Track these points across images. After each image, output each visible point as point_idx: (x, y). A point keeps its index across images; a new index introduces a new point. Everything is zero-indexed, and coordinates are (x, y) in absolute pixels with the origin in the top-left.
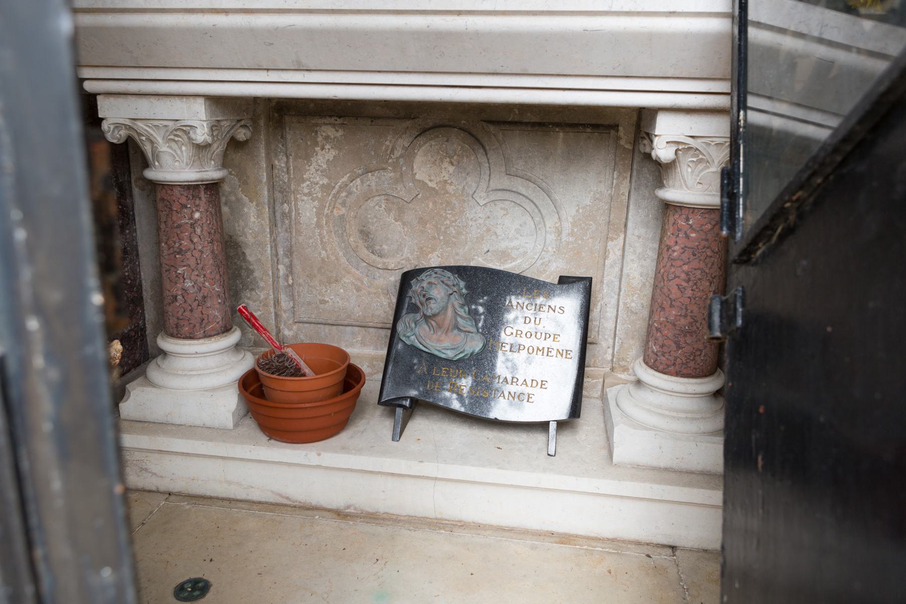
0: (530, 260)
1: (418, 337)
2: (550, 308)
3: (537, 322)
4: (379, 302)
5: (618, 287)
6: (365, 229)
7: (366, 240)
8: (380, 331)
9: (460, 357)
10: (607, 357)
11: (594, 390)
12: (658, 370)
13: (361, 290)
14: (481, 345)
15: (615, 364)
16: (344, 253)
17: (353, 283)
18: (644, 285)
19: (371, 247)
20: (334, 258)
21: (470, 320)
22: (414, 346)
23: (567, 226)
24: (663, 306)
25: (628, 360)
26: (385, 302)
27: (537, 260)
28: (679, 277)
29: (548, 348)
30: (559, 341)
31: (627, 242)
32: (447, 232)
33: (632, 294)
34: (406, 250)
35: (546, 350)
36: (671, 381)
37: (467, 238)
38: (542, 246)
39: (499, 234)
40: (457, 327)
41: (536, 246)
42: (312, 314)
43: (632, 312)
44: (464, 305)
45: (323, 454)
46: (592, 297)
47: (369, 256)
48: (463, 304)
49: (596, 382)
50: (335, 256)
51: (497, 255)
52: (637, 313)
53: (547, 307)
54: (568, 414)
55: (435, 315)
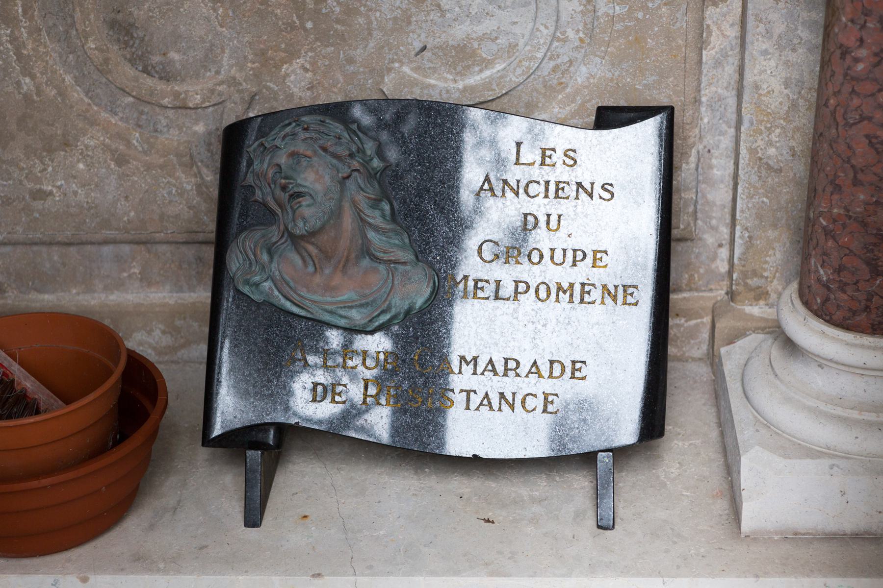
0: (524, 63)
1: (279, 284)
2: (580, 190)
3: (553, 224)
4: (175, 186)
5: (734, 109)
6: (120, 17)
7: (126, 43)
8: (184, 248)
9: (381, 322)
10: (717, 267)
11: (692, 342)
13: (128, 162)
14: (427, 292)
15: (737, 285)
16: (75, 77)
17: (106, 148)
18: (794, 106)
19: (141, 58)
20: (54, 92)
21: (397, 233)
22: (272, 305)
24: (837, 182)
25: (765, 274)
26: (188, 183)
27: (541, 63)
28: (870, 119)
29: (583, 285)
30: (606, 266)
31: (750, 12)
32: (321, 9)
33: (768, 129)
34: (226, 60)
35: (577, 289)
36: (862, 346)
37: (370, 22)
38: (552, 29)
39: (447, 7)
40: (366, 251)
41: (538, 30)
42: (15, 224)
43: (769, 168)
44: (380, 200)
45: (93, 579)
46: (675, 137)
47: (137, 81)
48: (375, 200)
49: (697, 325)
50: (55, 87)
51: (445, 55)
52: (780, 170)
53: (574, 187)
54: (638, 432)
55: (313, 234)
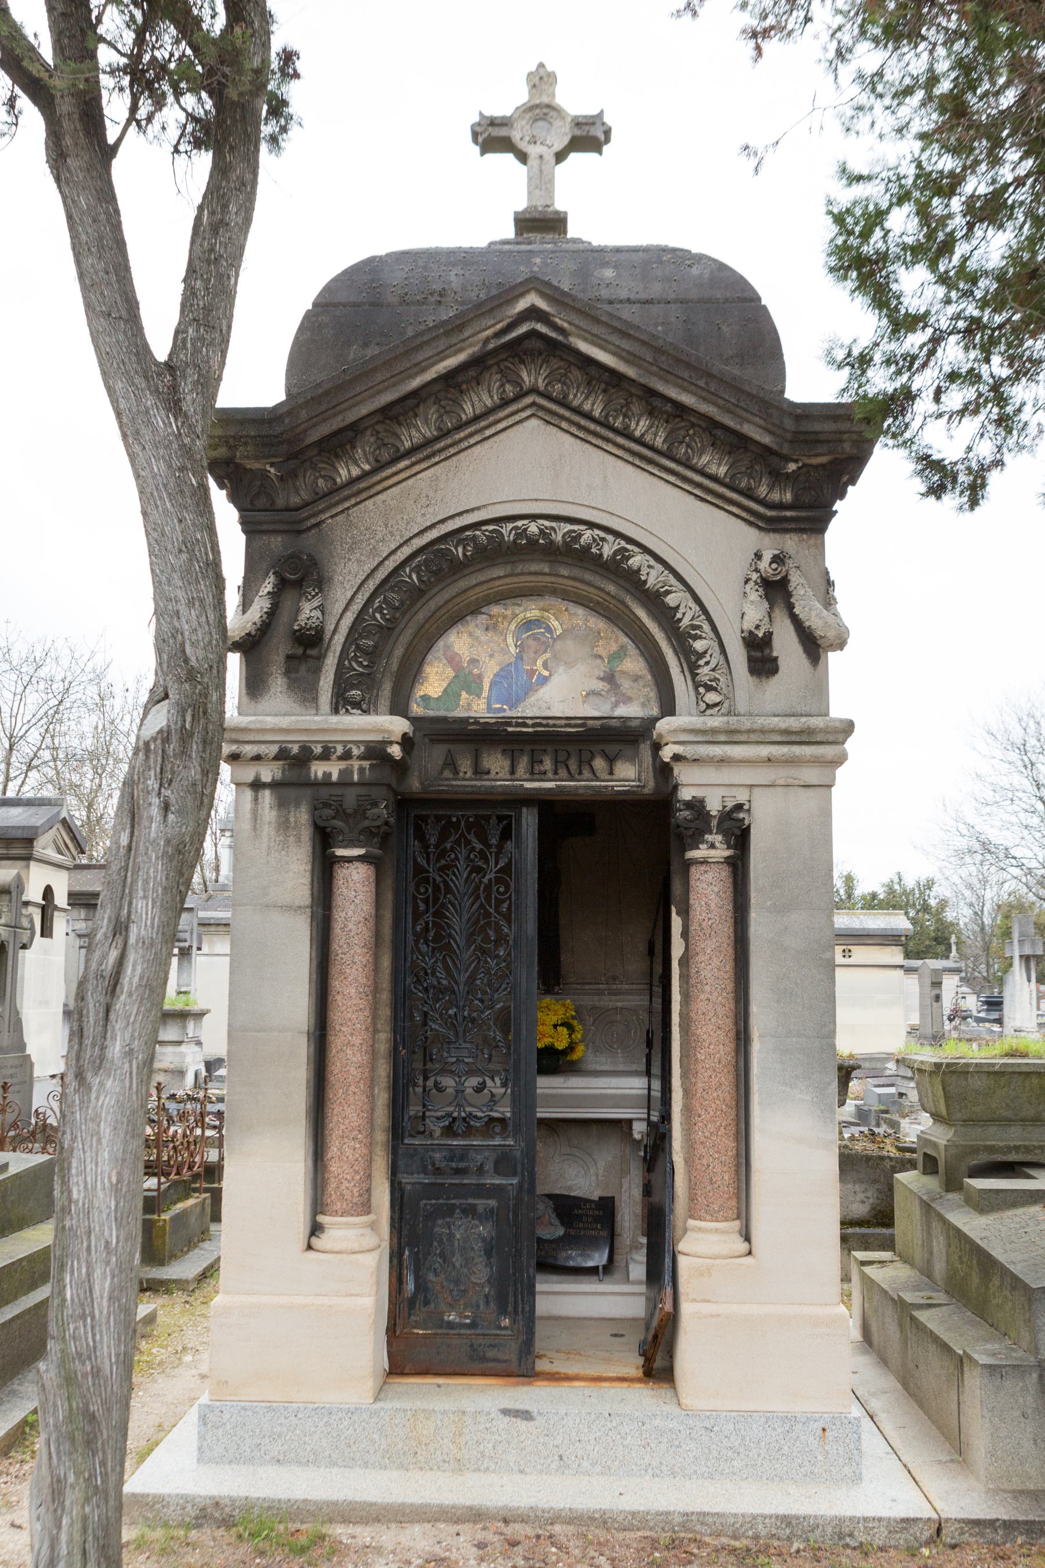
23: (601, 1172)
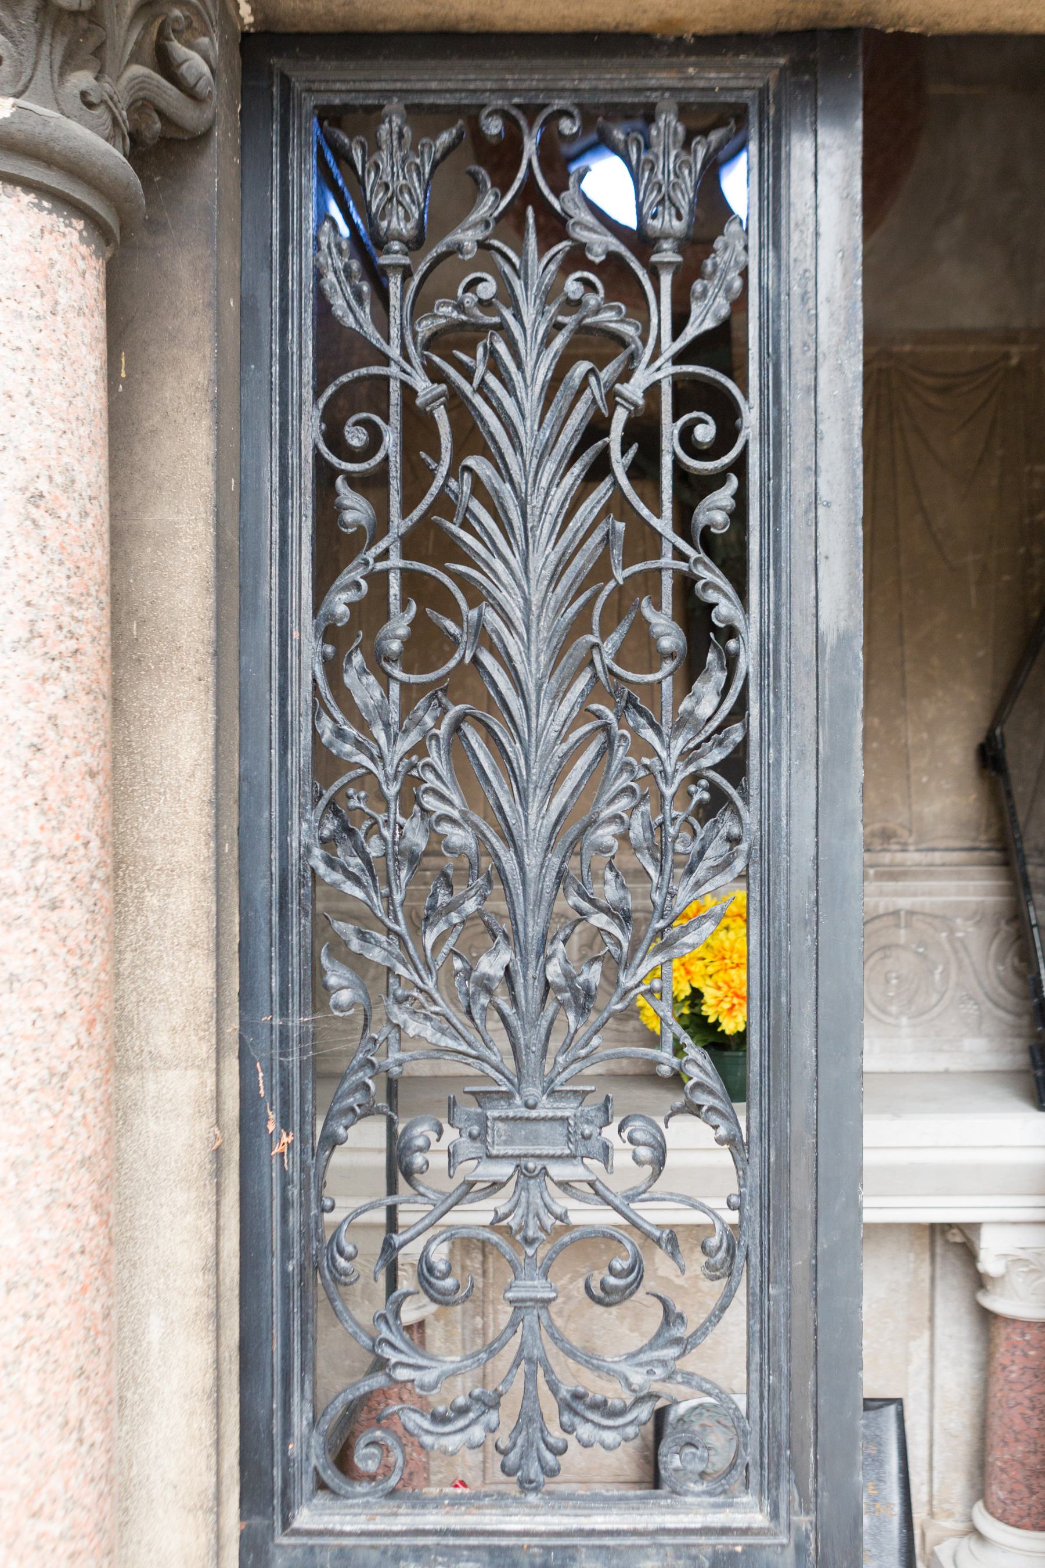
12: (1008, 1524)
